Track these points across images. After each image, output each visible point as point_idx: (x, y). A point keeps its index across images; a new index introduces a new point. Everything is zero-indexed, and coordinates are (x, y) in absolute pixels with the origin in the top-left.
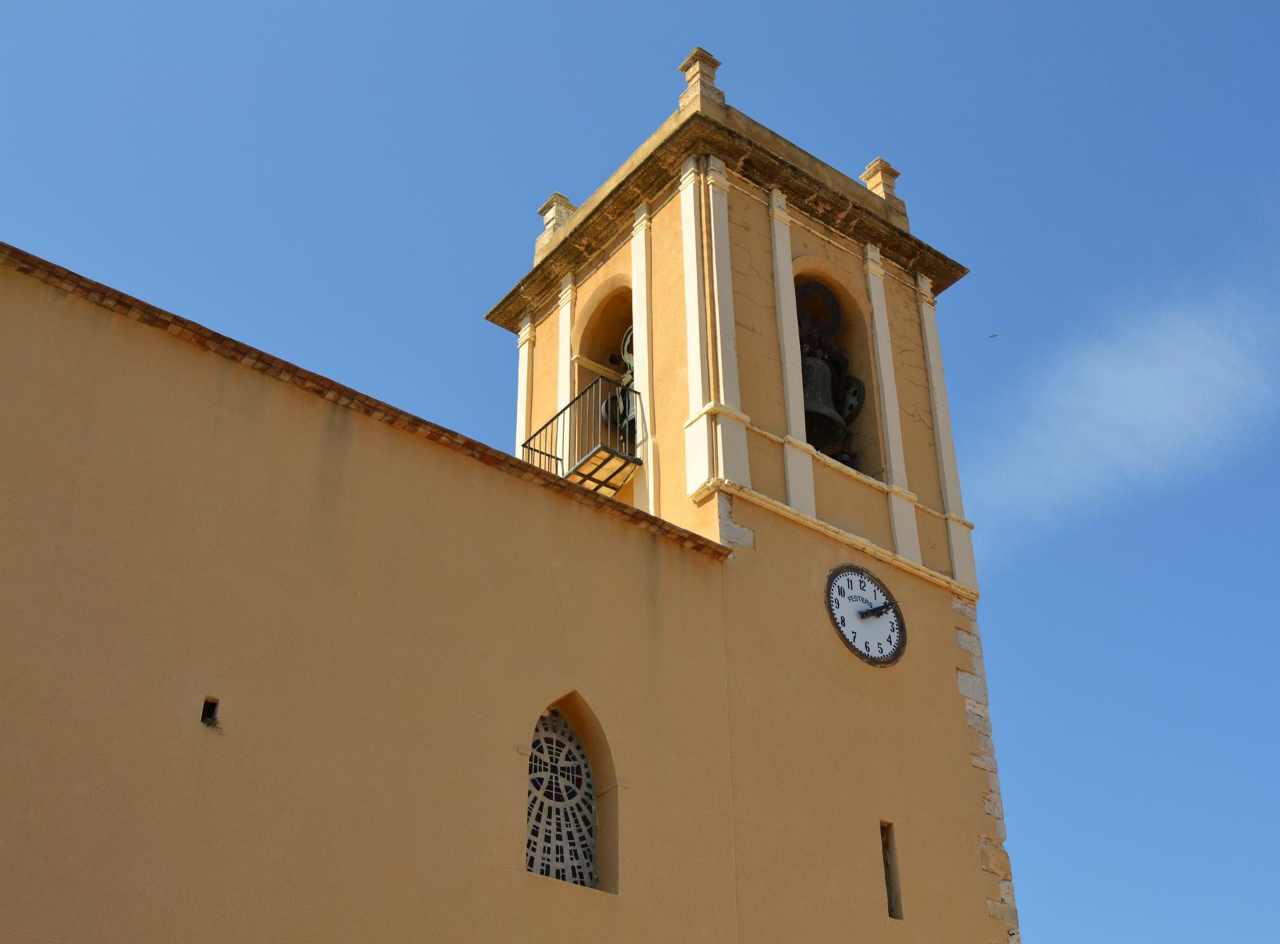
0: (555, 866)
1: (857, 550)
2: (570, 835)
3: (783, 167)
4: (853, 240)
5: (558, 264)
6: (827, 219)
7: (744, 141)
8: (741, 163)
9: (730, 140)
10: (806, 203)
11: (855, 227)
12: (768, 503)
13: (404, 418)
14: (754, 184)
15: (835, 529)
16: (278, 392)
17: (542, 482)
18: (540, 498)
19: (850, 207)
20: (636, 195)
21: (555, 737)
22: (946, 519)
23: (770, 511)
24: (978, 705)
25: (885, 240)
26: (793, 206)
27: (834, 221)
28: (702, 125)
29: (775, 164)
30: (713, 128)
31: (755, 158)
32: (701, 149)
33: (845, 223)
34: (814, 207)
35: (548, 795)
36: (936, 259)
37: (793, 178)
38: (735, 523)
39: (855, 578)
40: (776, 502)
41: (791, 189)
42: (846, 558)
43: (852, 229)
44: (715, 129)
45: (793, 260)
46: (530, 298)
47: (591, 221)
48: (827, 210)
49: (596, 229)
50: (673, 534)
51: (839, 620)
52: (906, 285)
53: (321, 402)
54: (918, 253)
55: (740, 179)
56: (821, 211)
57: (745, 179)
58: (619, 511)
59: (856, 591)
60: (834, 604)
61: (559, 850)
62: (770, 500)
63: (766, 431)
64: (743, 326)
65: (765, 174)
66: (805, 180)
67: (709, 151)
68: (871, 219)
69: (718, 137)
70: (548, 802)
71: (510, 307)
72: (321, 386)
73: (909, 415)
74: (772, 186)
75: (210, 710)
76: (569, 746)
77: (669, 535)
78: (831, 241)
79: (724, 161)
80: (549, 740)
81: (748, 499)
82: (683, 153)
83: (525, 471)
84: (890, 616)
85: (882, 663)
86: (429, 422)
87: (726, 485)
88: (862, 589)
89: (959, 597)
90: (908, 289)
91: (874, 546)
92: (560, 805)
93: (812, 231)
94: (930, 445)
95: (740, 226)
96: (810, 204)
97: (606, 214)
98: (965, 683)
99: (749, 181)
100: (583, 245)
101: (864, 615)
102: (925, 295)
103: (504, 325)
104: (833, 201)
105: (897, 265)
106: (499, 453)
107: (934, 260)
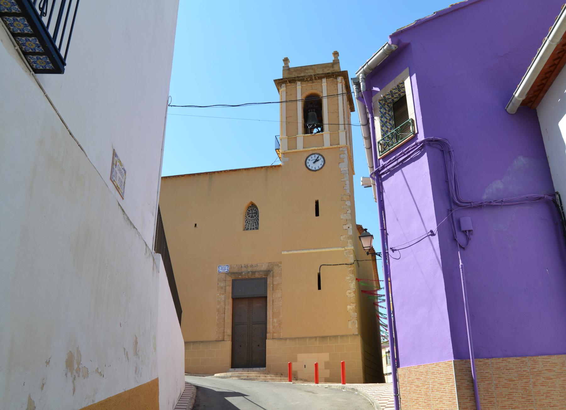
0: (252, 228)
1: (314, 150)
2: (255, 222)
6: (311, 80)
8: (288, 82)
16: (201, 177)
18: (244, 172)
21: (252, 208)
35: (251, 218)
42: (311, 153)
53: (208, 175)
56: (309, 80)
61: (253, 225)
68: (319, 75)
70: (251, 219)
72: (207, 173)
75: (196, 225)
76: (255, 209)
80: (251, 209)
89: (342, 147)
92: (253, 218)
101: (314, 163)
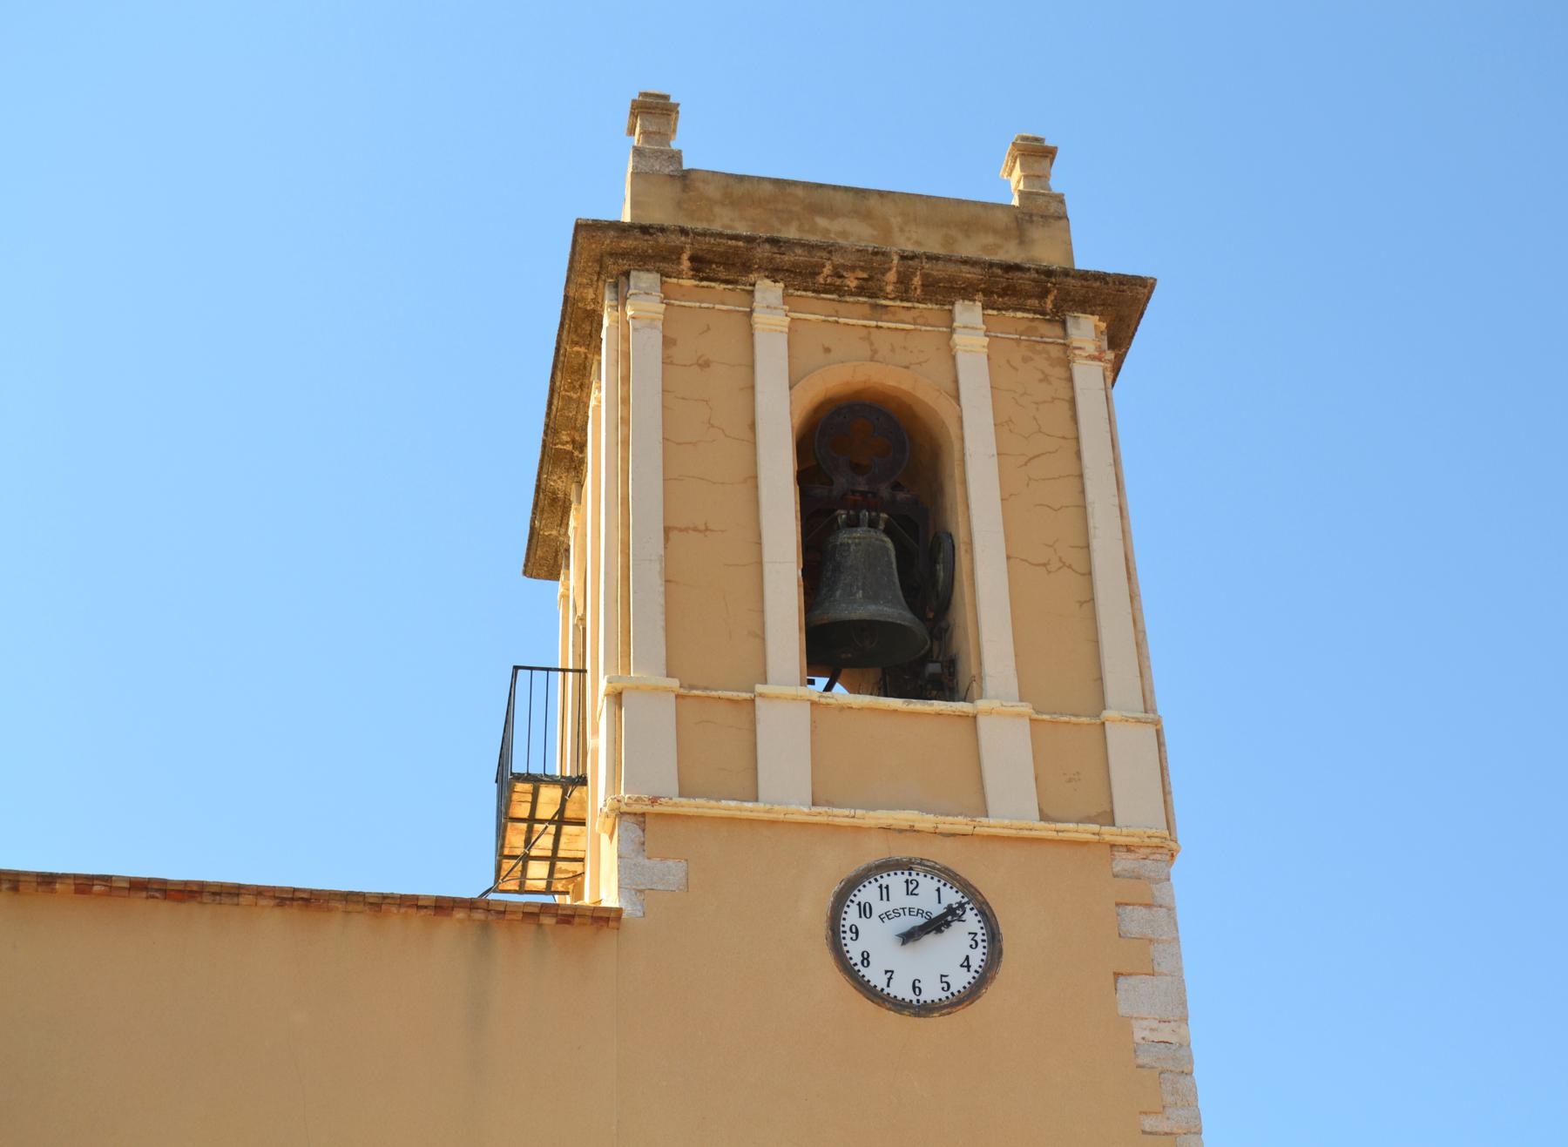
1: (901, 831)
3: (754, 245)
4: (930, 306)
5: (555, 478)
6: (870, 289)
7: (673, 232)
8: (686, 264)
9: (647, 240)
10: (822, 281)
11: (923, 285)
12: (711, 808)
13: (28, 878)
14: (723, 286)
15: (846, 812)
17: (272, 903)
19: (895, 262)
20: (583, 356)
22: (1103, 724)
23: (722, 818)
24: (1162, 1025)
25: (983, 286)
26: (804, 293)
27: (881, 289)
28: (593, 237)
29: (737, 247)
30: (612, 233)
31: (702, 250)
32: (614, 269)
33: (902, 287)
34: (838, 282)
36: (1085, 283)
37: (778, 256)
38: (649, 858)
39: (896, 881)
40: (724, 803)
41: (787, 270)
43: (919, 291)
44: (616, 235)
45: (791, 388)
46: (554, 533)
47: (554, 408)
48: (863, 279)
49: (568, 417)
50: (514, 912)
51: (857, 959)
52: (1045, 343)
54: (1049, 285)
55: (697, 286)
56: (852, 283)
57: (705, 283)
58: (410, 906)
59: (899, 898)
60: (849, 935)
62: (712, 803)
63: (716, 690)
64: (686, 530)
65: (733, 265)
66: (799, 251)
67: (626, 267)
68: (940, 265)
69: (628, 243)
71: (538, 553)
73: (1039, 565)
74: (752, 277)
77: (508, 917)
78: (880, 324)
79: (657, 272)
81: (673, 812)
82: (598, 280)
83: (238, 895)
84: (972, 921)
85: (946, 1007)
86: (62, 874)
87: (626, 804)
88: (910, 893)
90: (1050, 347)
91: (931, 817)
93: (842, 320)
94: (1081, 603)
95: (691, 365)
96: (829, 280)
97: (563, 393)
98: (1135, 997)
99: (713, 284)
100: (567, 442)
101: (909, 937)
102: (1080, 348)
103: (547, 578)
104: (862, 264)
105: (1026, 315)
106: (186, 883)
107: (1082, 286)
